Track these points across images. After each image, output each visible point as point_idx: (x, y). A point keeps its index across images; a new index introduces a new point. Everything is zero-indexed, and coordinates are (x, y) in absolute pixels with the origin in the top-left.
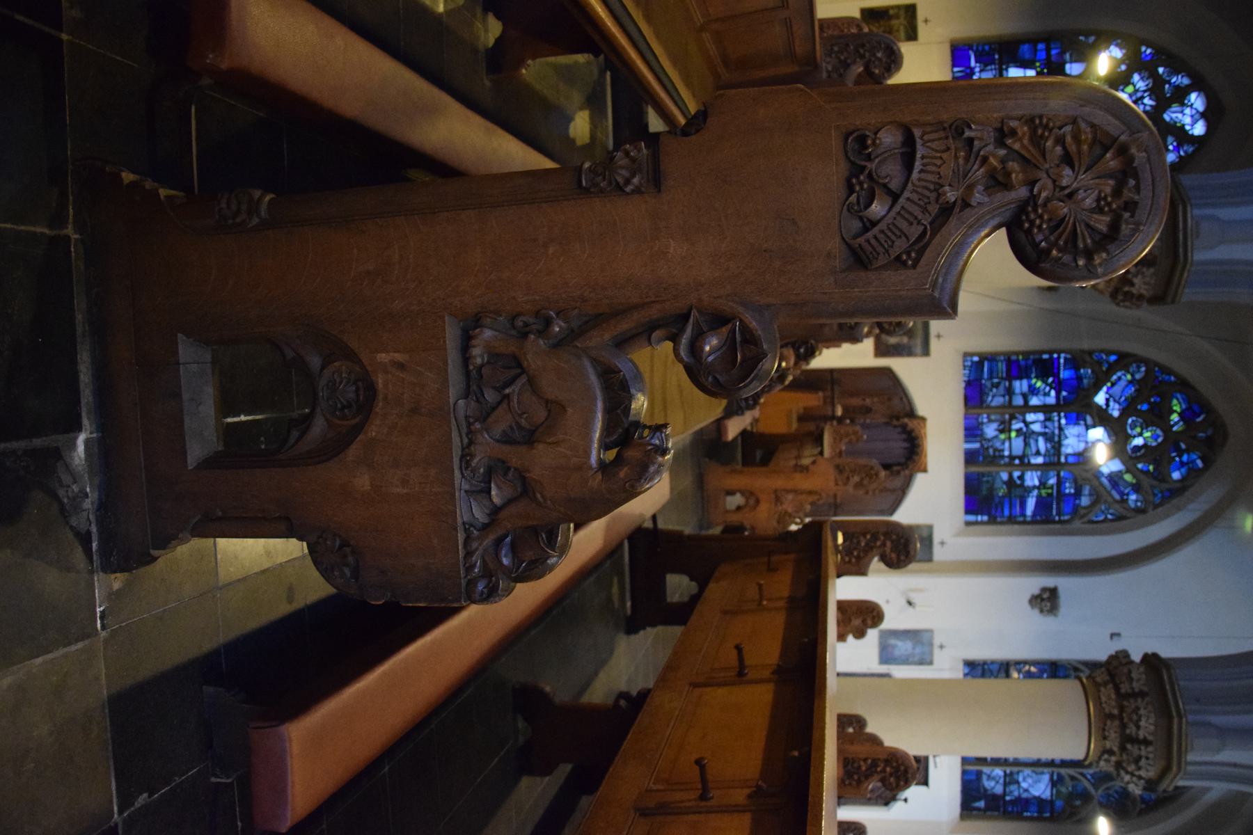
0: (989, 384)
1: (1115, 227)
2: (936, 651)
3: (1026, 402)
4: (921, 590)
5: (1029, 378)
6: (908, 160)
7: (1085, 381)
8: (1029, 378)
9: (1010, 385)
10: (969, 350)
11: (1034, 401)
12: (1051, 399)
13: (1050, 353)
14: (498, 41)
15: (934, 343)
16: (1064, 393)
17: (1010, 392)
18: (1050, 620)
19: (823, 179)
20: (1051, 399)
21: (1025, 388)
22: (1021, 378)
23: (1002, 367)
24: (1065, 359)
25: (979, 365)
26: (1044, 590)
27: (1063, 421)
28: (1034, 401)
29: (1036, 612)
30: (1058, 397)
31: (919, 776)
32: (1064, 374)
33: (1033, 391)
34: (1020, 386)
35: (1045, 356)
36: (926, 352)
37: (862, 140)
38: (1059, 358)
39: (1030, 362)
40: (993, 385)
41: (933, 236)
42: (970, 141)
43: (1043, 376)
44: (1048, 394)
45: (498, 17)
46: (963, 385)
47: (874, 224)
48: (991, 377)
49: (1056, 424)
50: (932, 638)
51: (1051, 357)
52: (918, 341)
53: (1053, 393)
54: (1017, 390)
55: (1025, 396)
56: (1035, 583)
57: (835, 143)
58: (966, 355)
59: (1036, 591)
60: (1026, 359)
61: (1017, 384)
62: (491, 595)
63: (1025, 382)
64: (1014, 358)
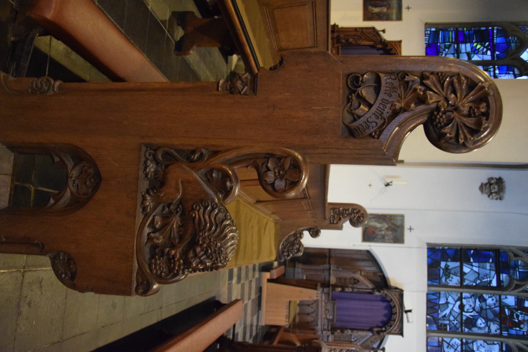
0: (442, 46)
1: (479, 124)
2: (407, 233)
3: (470, 58)
4: (396, 177)
5: (472, 43)
6: (377, 90)
7: (513, 45)
8: (472, 43)
9: (458, 46)
10: (430, 21)
11: (475, 58)
12: (488, 57)
13: (487, 24)
14: (182, 38)
15: (405, 12)
16: (497, 53)
17: (458, 52)
18: (496, 203)
19: (336, 93)
20: (488, 57)
21: (469, 49)
22: (465, 43)
23: (452, 35)
24: (497, 30)
25: (436, 33)
26: (490, 179)
27: (497, 72)
28: (475, 58)
29: (485, 196)
30: (492, 55)
31: (395, 328)
32: (497, 40)
33: (475, 51)
34: (465, 48)
35: (483, 29)
36: (399, 18)
37: (356, 79)
38: (493, 29)
39: (472, 32)
40: (445, 47)
41: (389, 123)
42: (408, 82)
43: (481, 41)
44: (485, 53)
45: (183, 29)
46: (425, 46)
47: (359, 117)
48: (444, 41)
49: (492, 74)
50: (403, 220)
51: (487, 30)
52: (394, 12)
53: (489, 53)
54: (463, 51)
55: (468, 54)
56: (484, 175)
57: (341, 83)
58: (427, 25)
59: (485, 181)
60: (469, 30)
61: (463, 47)
62: (145, 289)
63: (468, 45)
64: (460, 29)
